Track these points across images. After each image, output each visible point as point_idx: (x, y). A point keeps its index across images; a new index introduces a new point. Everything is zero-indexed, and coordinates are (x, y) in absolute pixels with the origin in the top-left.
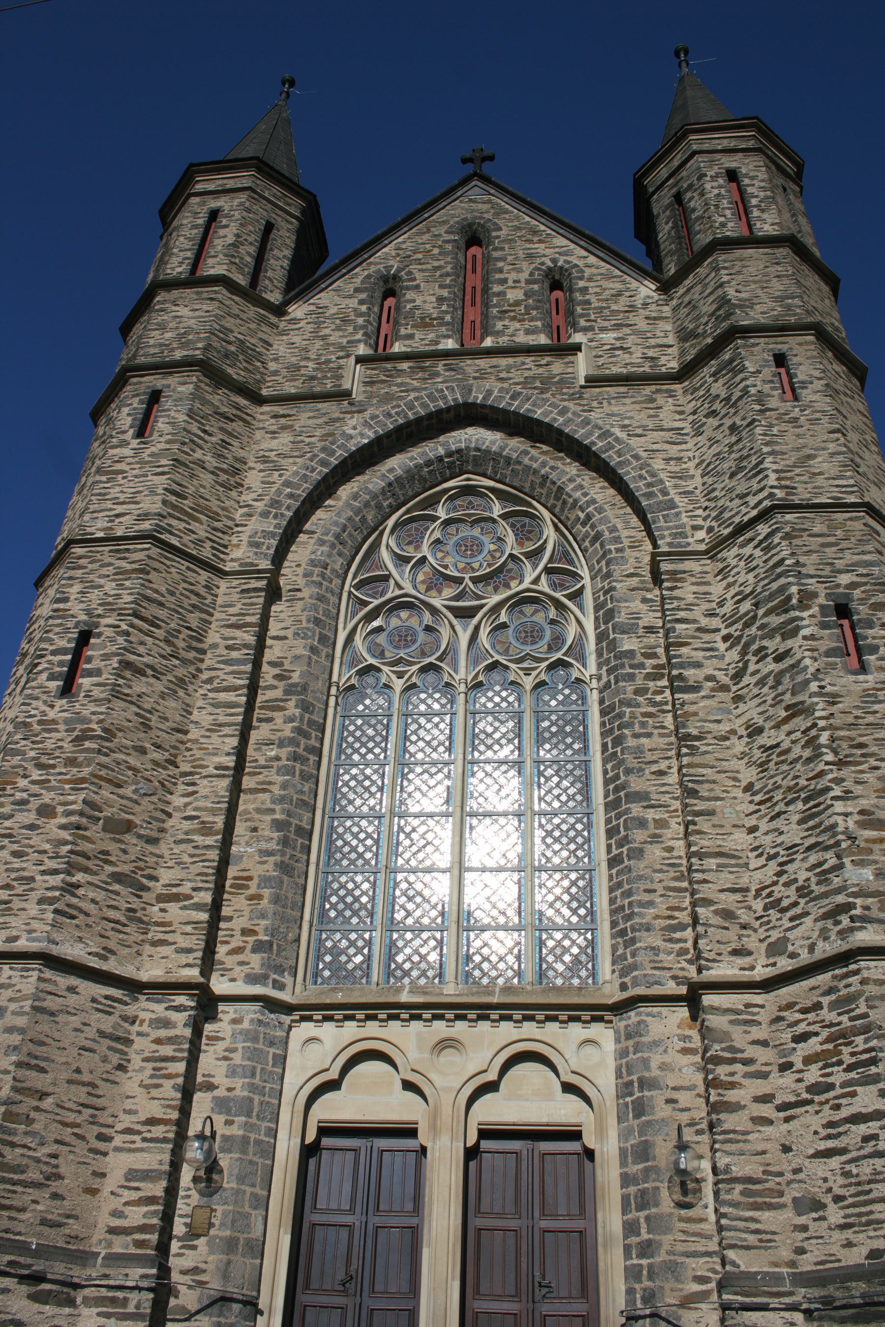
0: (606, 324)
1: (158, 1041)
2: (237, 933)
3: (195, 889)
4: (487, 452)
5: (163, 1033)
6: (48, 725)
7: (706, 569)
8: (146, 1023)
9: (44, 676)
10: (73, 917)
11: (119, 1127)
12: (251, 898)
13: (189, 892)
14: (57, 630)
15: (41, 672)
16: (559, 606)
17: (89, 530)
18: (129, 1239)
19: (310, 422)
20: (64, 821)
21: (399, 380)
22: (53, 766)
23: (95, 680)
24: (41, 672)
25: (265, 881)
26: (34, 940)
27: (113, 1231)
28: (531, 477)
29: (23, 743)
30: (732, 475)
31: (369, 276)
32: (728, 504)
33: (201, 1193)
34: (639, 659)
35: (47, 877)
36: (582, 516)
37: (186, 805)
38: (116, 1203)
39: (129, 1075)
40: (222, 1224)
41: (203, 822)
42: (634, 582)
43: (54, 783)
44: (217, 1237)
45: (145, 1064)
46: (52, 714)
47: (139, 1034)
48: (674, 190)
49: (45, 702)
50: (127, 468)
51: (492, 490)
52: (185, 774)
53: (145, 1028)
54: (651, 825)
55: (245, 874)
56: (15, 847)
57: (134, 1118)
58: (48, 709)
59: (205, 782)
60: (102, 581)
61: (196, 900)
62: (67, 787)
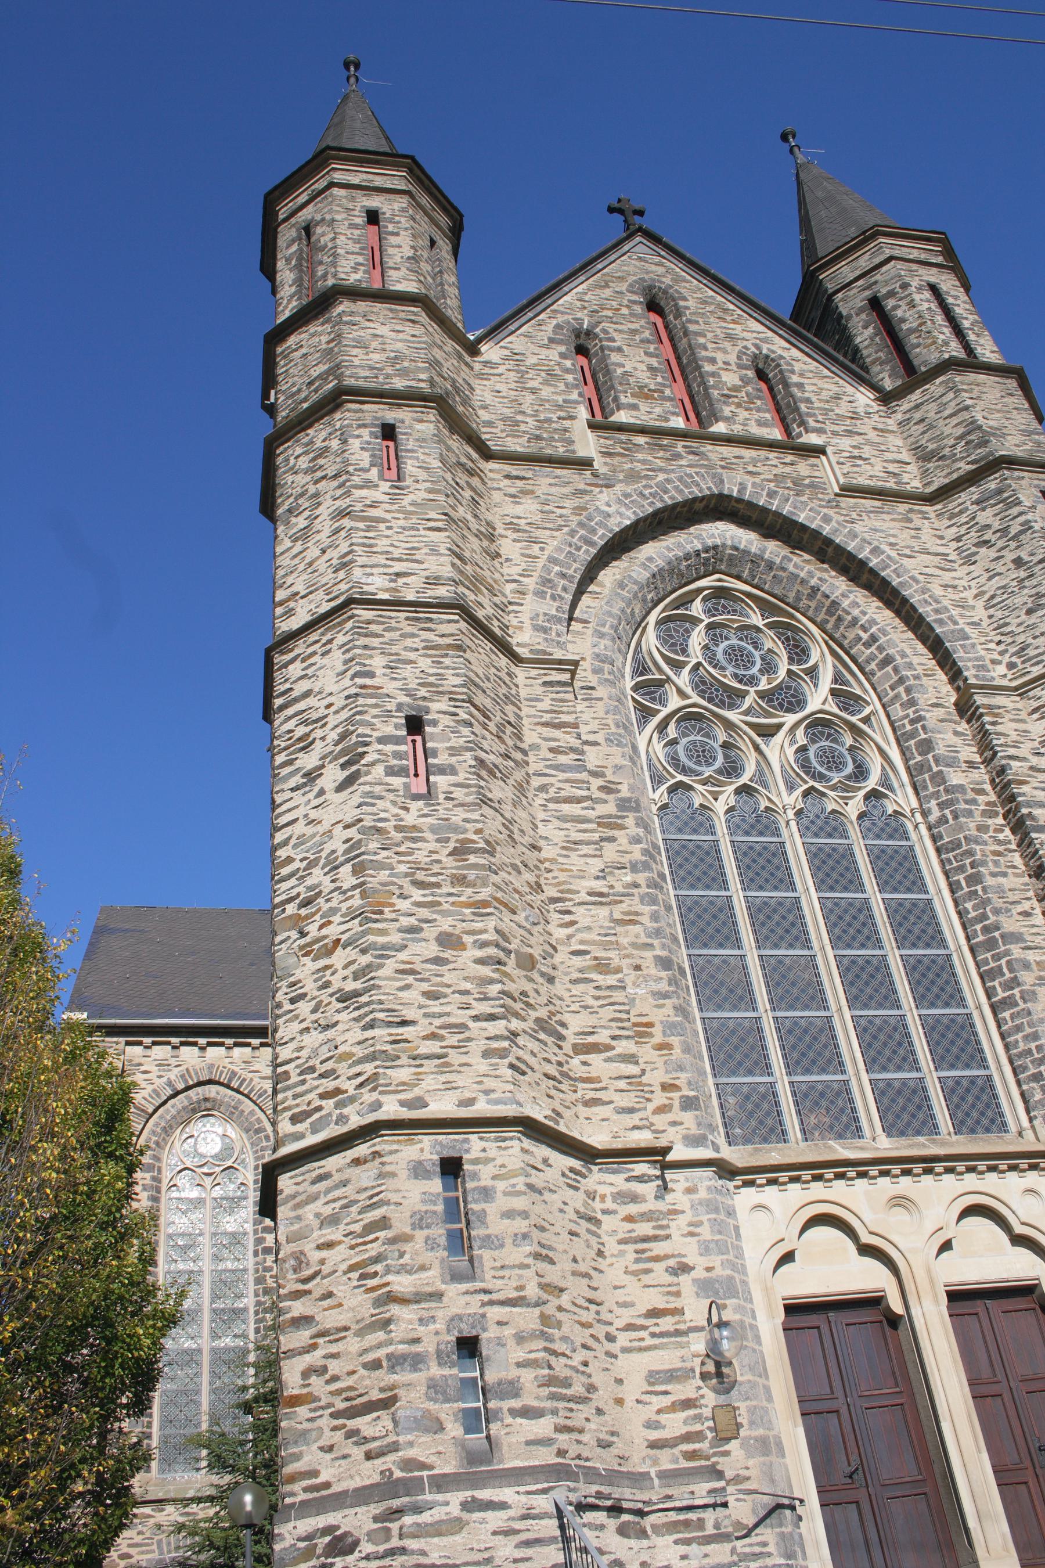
0: (836, 428)
1: (629, 1219)
2: (657, 1088)
3: (613, 1038)
4: (746, 552)
5: (633, 1209)
6: (413, 834)
7: (1019, 705)
8: (609, 1199)
9: (379, 770)
10: (524, 1073)
11: (620, 1323)
12: (660, 1047)
13: (608, 1041)
14: (374, 711)
15: (373, 764)
16: (853, 728)
17: (366, 588)
18: (676, 1451)
19: (553, 490)
20: (479, 953)
21: (640, 456)
22: (438, 885)
23: (452, 779)
24: (373, 764)
25: (670, 1028)
26: (497, 1102)
27: (653, 1445)
28: (797, 587)
29: (385, 853)
30: (1029, 612)
31: (558, 326)
32: (1030, 640)
33: (717, 1392)
34: (970, 795)
35: (484, 1024)
36: (865, 636)
37: (569, 937)
38: (648, 1412)
39: (609, 1260)
40: (752, 1423)
41: (596, 958)
42: (940, 712)
43: (446, 907)
44: (750, 1438)
45: (622, 1247)
46: (410, 819)
47: (605, 1212)
48: (867, 293)
49: (394, 803)
50: (388, 516)
51: (749, 595)
52: (554, 900)
53: (609, 1204)
54: (1034, 966)
55: (644, 1020)
56: (425, 986)
57: (631, 1311)
58: (402, 812)
59: (581, 910)
60: (412, 656)
61: (618, 1050)
62: (467, 911)
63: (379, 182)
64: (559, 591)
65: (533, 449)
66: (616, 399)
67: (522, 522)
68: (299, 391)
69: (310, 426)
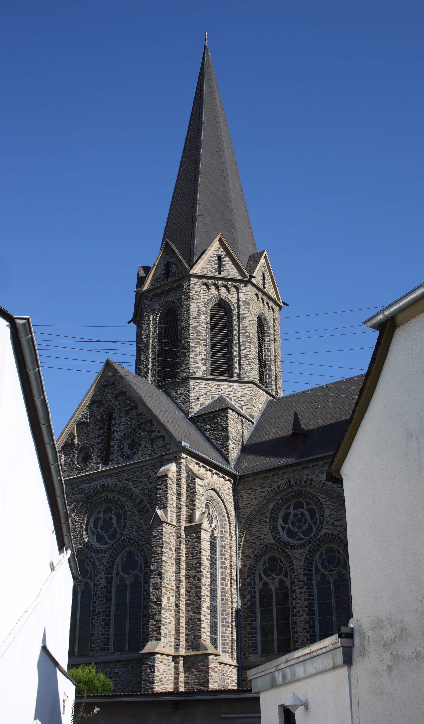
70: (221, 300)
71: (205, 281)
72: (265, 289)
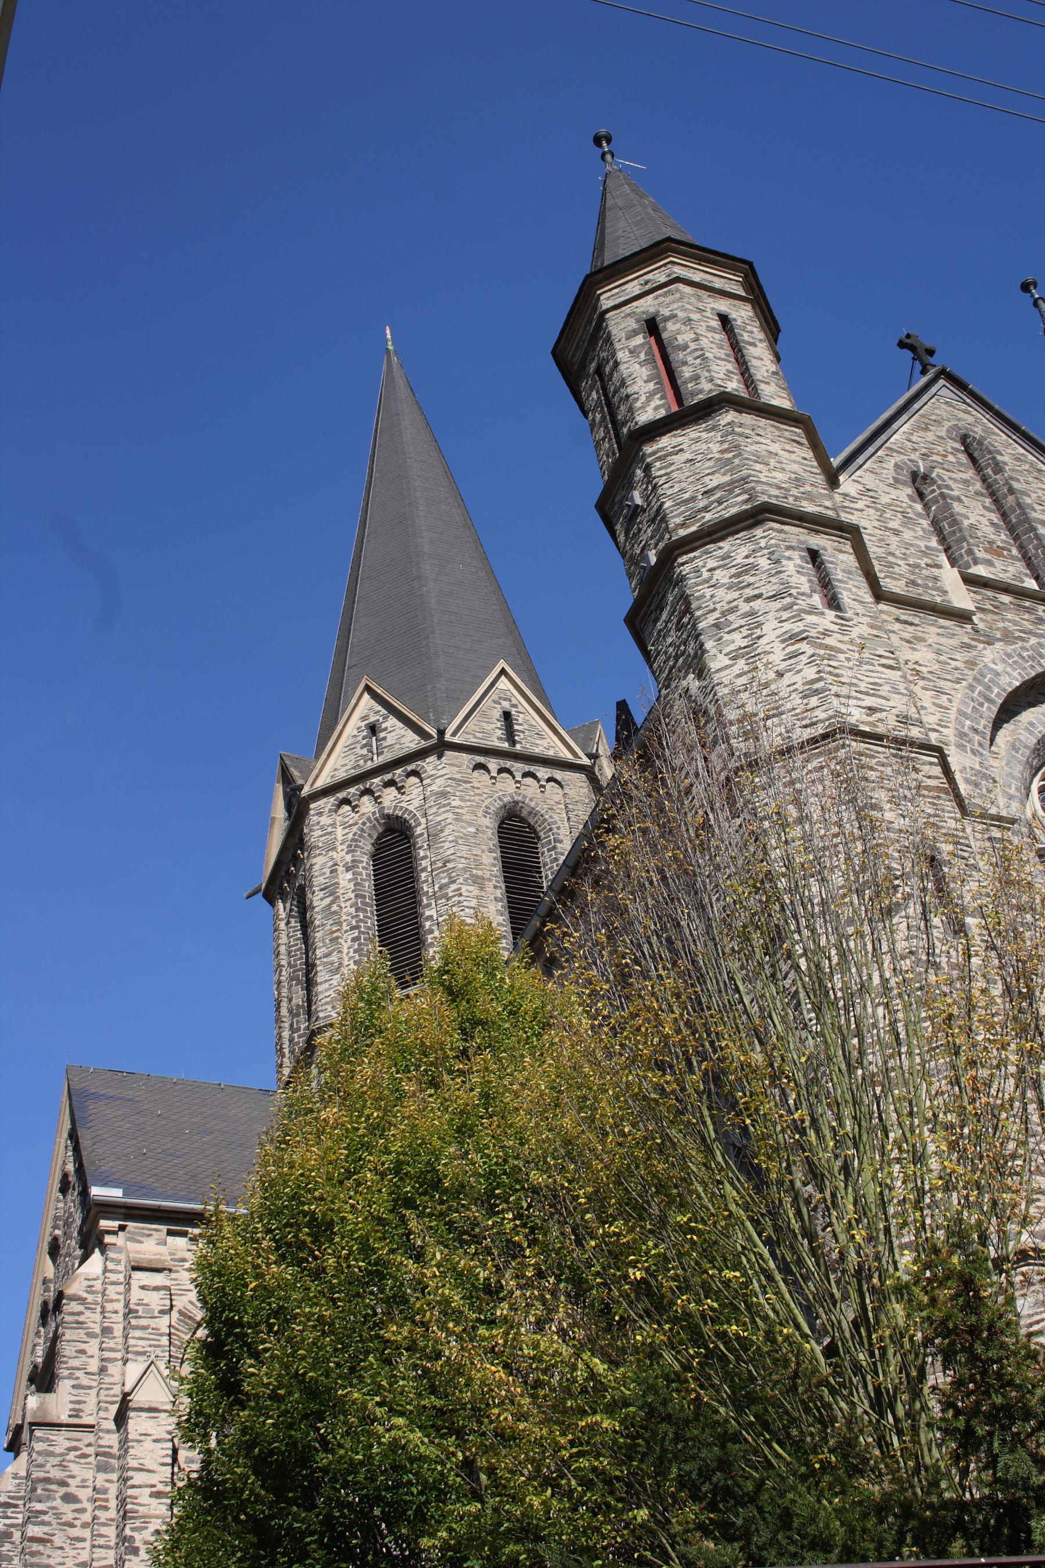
19: (943, 640)
63: (718, 283)
64: (976, 747)
65: (913, 593)
66: (970, 552)
67: (924, 670)
68: (693, 499)
69: (722, 538)
70: (388, 817)
71: (341, 795)
72: (518, 747)
